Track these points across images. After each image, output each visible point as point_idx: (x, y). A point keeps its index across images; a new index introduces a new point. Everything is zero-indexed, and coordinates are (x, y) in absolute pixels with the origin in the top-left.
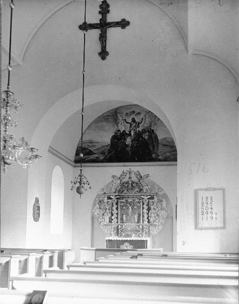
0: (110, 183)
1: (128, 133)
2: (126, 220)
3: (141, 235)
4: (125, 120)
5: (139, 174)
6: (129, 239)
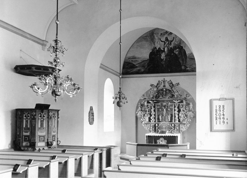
0: (148, 91)
1: (163, 49)
2: (162, 119)
3: (173, 132)
4: (160, 39)
5: (172, 83)
6: (163, 135)
